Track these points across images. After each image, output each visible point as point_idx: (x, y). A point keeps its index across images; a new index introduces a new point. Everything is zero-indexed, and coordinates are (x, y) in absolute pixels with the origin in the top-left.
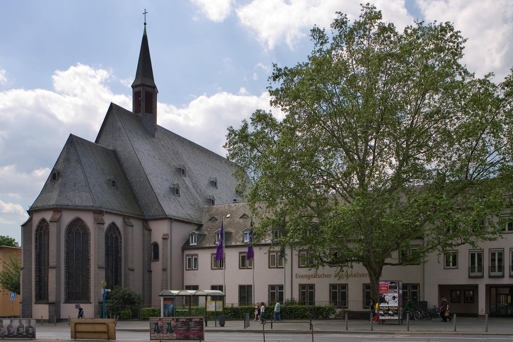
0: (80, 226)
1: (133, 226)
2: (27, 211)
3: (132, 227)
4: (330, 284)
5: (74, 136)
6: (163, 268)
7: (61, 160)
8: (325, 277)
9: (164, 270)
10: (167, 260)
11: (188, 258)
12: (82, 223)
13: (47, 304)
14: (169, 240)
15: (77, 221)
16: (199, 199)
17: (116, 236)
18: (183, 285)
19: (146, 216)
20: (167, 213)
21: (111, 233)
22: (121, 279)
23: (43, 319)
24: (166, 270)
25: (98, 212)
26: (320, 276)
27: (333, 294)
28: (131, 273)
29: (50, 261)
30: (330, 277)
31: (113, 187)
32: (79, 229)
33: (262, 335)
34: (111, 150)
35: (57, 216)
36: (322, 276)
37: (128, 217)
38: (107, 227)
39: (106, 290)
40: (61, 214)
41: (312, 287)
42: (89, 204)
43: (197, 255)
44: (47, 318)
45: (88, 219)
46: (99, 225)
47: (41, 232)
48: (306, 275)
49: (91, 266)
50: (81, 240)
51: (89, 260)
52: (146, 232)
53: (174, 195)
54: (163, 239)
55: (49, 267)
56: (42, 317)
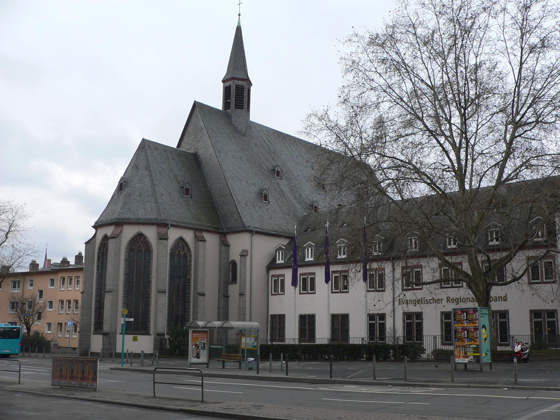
0: (142, 242)
1: (205, 241)
2: (93, 227)
3: (204, 242)
4: (530, 310)
5: (147, 140)
6: (240, 292)
7: (131, 168)
8: (501, 301)
9: (242, 294)
10: (245, 282)
11: (274, 280)
12: (144, 239)
13: (101, 334)
14: (248, 258)
15: (140, 235)
16: (296, 205)
17: (185, 253)
18: (268, 314)
19: (224, 229)
20: (247, 224)
21: (178, 250)
22: (190, 305)
23: (129, 352)
24: (243, 295)
25: (162, 225)
26: (428, 301)
27: (535, 326)
28: (200, 298)
29: (106, 284)
30: (441, 303)
31: (186, 196)
32: (142, 245)
33: (152, 375)
34: (191, 153)
35: (118, 231)
36: (431, 301)
37: (201, 230)
38: (173, 243)
39: (127, 319)
40: (121, 231)
41: (419, 316)
42: (153, 216)
43: (313, 274)
44: (117, 352)
45: (151, 233)
46: (161, 241)
47: (103, 250)
48: (501, 297)
49: (152, 289)
50: (143, 258)
51: (150, 282)
52: (223, 248)
53: (261, 201)
54: (241, 256)
55: (106, 291)
56: (128, 350)
